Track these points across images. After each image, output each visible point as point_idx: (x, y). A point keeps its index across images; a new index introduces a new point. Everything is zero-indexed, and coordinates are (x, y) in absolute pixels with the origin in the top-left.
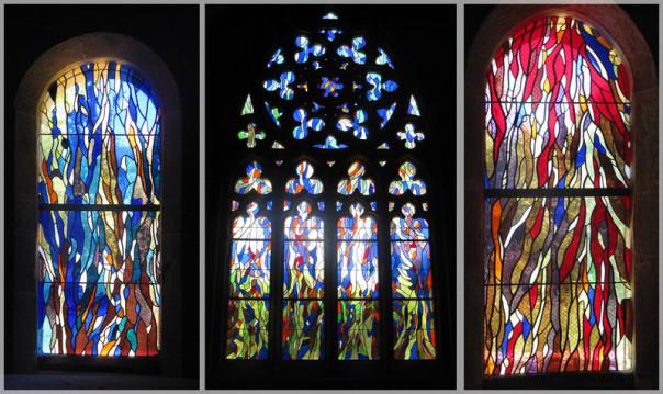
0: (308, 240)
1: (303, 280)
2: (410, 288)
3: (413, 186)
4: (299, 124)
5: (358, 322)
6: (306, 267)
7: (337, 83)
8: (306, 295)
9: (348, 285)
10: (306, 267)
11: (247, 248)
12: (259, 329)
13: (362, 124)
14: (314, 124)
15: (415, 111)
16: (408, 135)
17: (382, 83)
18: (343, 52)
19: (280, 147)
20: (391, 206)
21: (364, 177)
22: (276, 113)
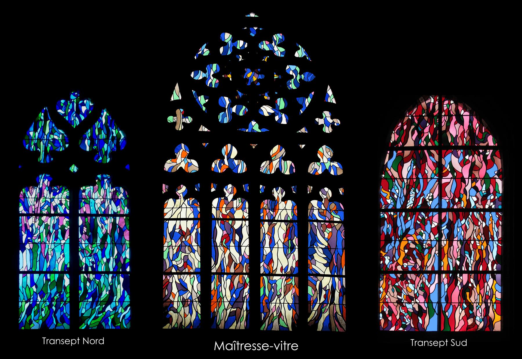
0: (234, 220)
1: (230, 255)
2: (325, 265)
3: (330, 166)
4: (224, 110)
5: (279, 296)
6: (232, 244)
7: (259, 73)
8: (232, 270)
9: (270, 261)
10: (232, 244)
11: (177, 227)
12: (192, 301)
13: (282, 111)
14: (238, 110)
15: (332, 100)
16: (326, 120)
17: (300, 74)
18: (265, 46)
19: (206, 130)
20: (310, 188)
21: (285, 158)
22: (202, 100)
